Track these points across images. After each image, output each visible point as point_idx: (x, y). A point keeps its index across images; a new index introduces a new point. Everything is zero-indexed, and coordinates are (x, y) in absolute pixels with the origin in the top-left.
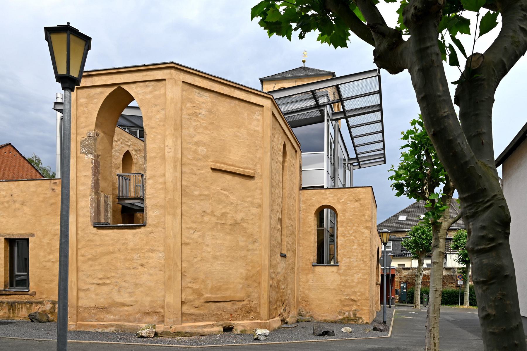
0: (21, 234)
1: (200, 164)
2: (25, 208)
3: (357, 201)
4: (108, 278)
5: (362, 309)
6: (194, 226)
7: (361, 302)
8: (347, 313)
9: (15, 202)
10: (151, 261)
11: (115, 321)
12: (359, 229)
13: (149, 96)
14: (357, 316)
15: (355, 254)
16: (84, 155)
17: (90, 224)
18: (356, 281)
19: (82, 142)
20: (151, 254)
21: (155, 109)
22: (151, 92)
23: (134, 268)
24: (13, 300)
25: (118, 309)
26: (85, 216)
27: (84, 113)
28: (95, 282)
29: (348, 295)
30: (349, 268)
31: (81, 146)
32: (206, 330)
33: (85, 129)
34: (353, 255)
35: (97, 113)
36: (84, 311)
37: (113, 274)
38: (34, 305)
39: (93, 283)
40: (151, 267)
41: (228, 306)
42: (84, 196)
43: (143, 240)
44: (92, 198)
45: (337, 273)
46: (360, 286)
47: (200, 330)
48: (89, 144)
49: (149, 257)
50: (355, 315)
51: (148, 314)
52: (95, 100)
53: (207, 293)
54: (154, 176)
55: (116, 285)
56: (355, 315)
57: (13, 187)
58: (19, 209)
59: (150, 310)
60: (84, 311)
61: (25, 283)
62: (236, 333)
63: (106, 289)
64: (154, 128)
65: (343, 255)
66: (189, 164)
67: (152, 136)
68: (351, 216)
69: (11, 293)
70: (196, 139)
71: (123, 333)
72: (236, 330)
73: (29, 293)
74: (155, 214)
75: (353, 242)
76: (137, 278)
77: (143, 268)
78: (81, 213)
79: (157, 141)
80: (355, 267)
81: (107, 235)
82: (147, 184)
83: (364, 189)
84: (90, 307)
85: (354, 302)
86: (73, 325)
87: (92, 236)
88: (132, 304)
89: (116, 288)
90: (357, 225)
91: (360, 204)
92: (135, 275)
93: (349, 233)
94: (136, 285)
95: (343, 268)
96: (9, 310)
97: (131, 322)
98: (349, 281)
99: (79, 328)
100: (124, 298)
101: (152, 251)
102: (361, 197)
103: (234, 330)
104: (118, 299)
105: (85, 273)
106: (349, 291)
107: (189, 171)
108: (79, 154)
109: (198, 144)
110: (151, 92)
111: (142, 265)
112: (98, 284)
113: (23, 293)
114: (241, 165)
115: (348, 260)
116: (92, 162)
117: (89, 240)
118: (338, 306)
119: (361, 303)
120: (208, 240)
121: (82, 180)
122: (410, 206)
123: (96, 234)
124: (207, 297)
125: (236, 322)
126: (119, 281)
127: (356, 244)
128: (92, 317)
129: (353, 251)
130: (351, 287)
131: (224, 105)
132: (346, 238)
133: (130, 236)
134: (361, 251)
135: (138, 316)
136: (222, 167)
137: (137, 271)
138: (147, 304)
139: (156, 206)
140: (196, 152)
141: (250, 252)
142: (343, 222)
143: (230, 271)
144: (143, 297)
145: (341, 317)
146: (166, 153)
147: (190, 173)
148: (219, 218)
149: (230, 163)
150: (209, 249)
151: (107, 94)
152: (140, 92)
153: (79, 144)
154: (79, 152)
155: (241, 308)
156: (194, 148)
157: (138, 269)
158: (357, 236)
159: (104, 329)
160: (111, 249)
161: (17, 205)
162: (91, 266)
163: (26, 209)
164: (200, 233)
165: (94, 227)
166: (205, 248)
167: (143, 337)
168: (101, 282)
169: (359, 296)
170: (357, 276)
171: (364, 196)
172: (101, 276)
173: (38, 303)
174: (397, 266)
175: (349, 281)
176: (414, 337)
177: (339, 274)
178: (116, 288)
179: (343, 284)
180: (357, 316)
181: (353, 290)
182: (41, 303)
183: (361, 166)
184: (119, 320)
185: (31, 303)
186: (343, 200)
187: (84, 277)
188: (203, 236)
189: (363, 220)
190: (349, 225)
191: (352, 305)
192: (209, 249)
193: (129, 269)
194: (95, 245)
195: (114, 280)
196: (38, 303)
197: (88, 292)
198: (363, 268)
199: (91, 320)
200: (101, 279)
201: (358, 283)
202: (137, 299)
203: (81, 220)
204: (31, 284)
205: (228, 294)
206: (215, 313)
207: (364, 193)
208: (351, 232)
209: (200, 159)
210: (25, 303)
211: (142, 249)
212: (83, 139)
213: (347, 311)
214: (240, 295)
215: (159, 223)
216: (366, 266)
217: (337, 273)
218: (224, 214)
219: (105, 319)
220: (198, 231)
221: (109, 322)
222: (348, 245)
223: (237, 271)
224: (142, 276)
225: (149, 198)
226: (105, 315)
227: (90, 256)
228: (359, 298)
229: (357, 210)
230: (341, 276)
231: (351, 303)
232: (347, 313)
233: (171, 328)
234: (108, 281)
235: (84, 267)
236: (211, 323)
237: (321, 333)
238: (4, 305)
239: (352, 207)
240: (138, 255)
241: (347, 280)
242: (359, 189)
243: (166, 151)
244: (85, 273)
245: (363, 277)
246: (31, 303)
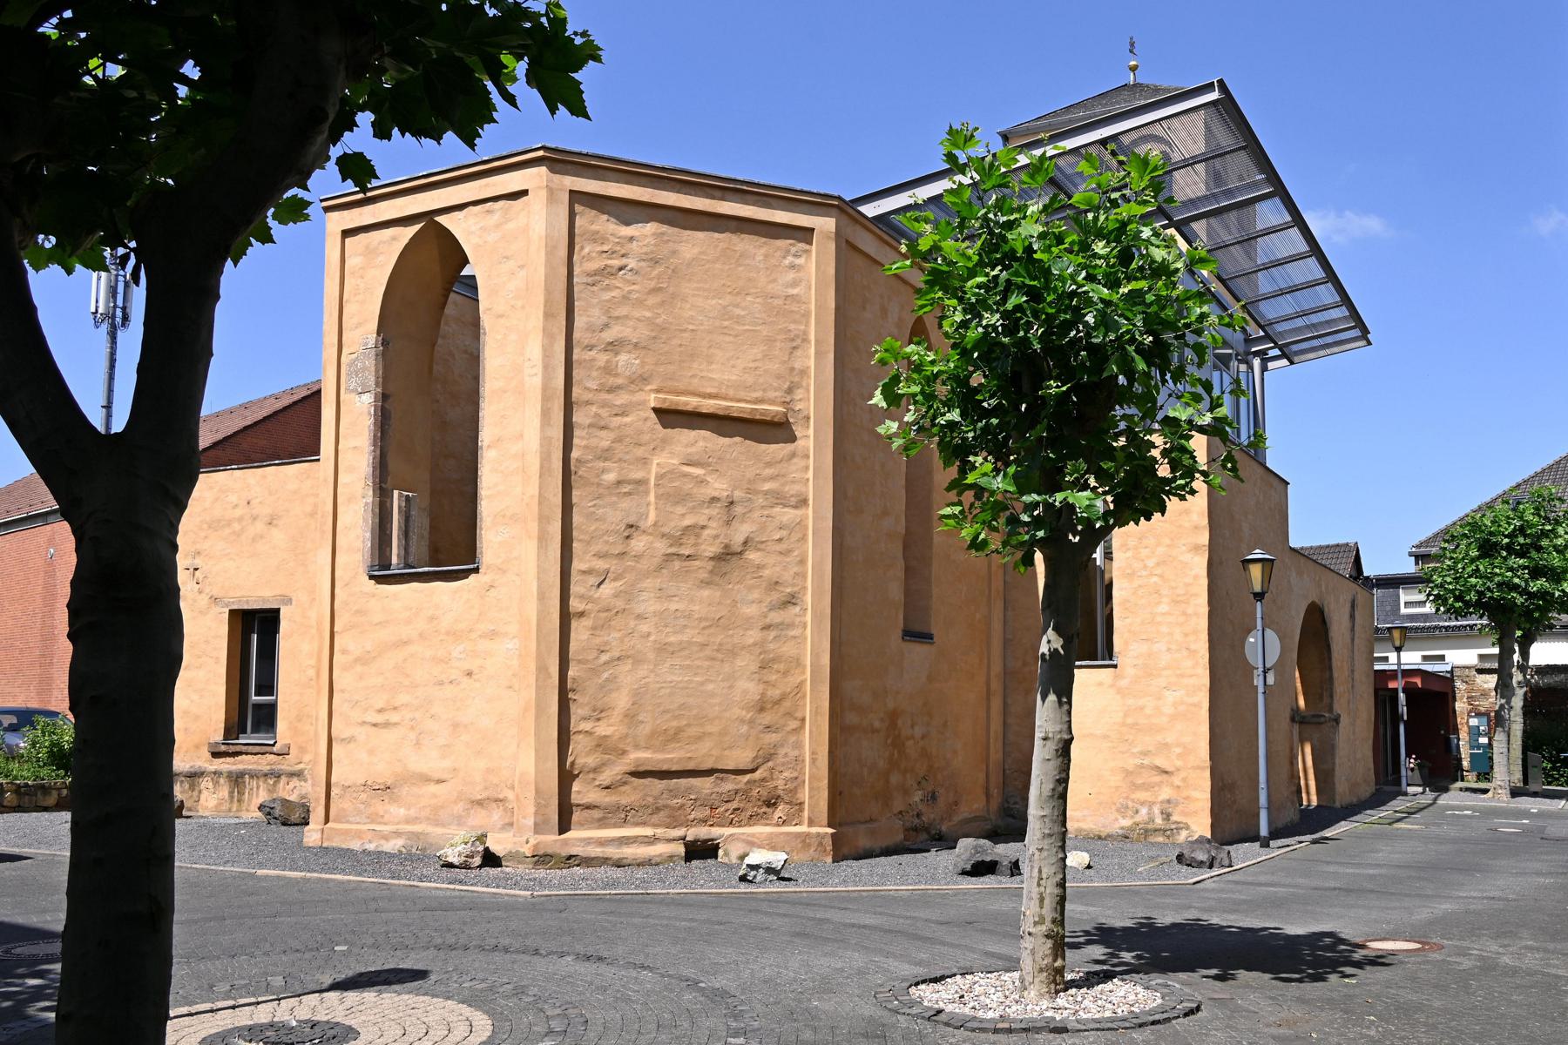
0: (264, 600)
1: (621, 399)
2: (275, 532)
6: (601, 565)
7: (1183, 774)
8: (1144, 811)
9: (255, 518)
11: (408, 822)
13: (492, 237)
14: (1174, 818)
18: (1168, 710)
19: (351, 364)
22: (498, 226)
24: (241, 767)
29: (1145, 754)
32: (630, 852)
38: (284, 779)
41: (705, 785)
45: (1112, 686)
47: (613, 852)
50: (1167, 816)
51: (480, 803)
52: (381, 258)
53: (637, 747)
55: (412, 728)
56: (1167, 816)
57: (252, 481)
58: (262, 537)
59: (484, 795)
61: (266, 718)
62: (726, 860)
63: (390, 736)
64: (501, 316)
66: (588, 403)
69: (238, 748)
70: (609, 336)
72: (726, 854)
73: (275, 749)
85: (1165, 776)
88: (443, 777)
89: (412, 736)
90: (1168, 541)
93: (1145, 567)
94: (455, 726)
96: (231, 793)
97: (443, 825)
98: (1148, 711)
101: (493, 635)
103: (721, 852)
107: (588, 421)
109: (614, 346)
111: (470, 674)
113: (264, 750)
114: (742, 394)
117: (358, 612)
118: (1117, 788)
119: (1184, 780)
120: (648, 604)
122: (1551, 467)
124: (637, 759)
126: (418, 715)
127: (1165, 600)
128: (360, 812)
129: (1159, 619)
131: (694, 244)
132: (1137, 583)
134: (1182, 619)
135: (459, 808)
136: (687, 404)
140: (608, 370)
141: (773, 634)
143: (710, 687)
145: (1127, 823)
147: (590, 426)
148: (677, 541)
149: (709, 390)
150: (644, 628)
151: (406, 241)
155: (746, 792)
156: (603, 358)
161: (260, 526)
163: (278, 536)
164: (618, 584)
165: (371, 577)
166: (632, 623)
168: (379, 719)
170: (1170, 697)
172: (380, 705)
173: (292, 775)
174: (1419, 660)
176: (1260, 885)
177: (1119, 691)
179: (1129, 721)
181: (1159, 738)
182: (298, 774)
183: (1296, 359)
184: (415, 820)
185: (278, 776)
188: (628, 594)
189: (1187, 524)
191: (1160, 784)
192: (644, 628)
193: (441, 683)
196: (292, 775)
197: (352, 745)
200: (380, 711)
204: (281, 725)
205: (703, 754)
206: (661, 803)
208: (1151, 563)
209: (619, 387)
210: (266, 775)
213: (1142, 804)
214: (741, 757)
217: (1112, 686)
220: (615, 580)
223: (731, 687)
228: (1179, 763)
231: (1157, 779)
232: (1144, 811)
234: (394, 717)
236: (649, 831)
237: (968, 867)
238: (222, 781)
240: (461, 648)
241: (1142, 708)
246: (278, 776)
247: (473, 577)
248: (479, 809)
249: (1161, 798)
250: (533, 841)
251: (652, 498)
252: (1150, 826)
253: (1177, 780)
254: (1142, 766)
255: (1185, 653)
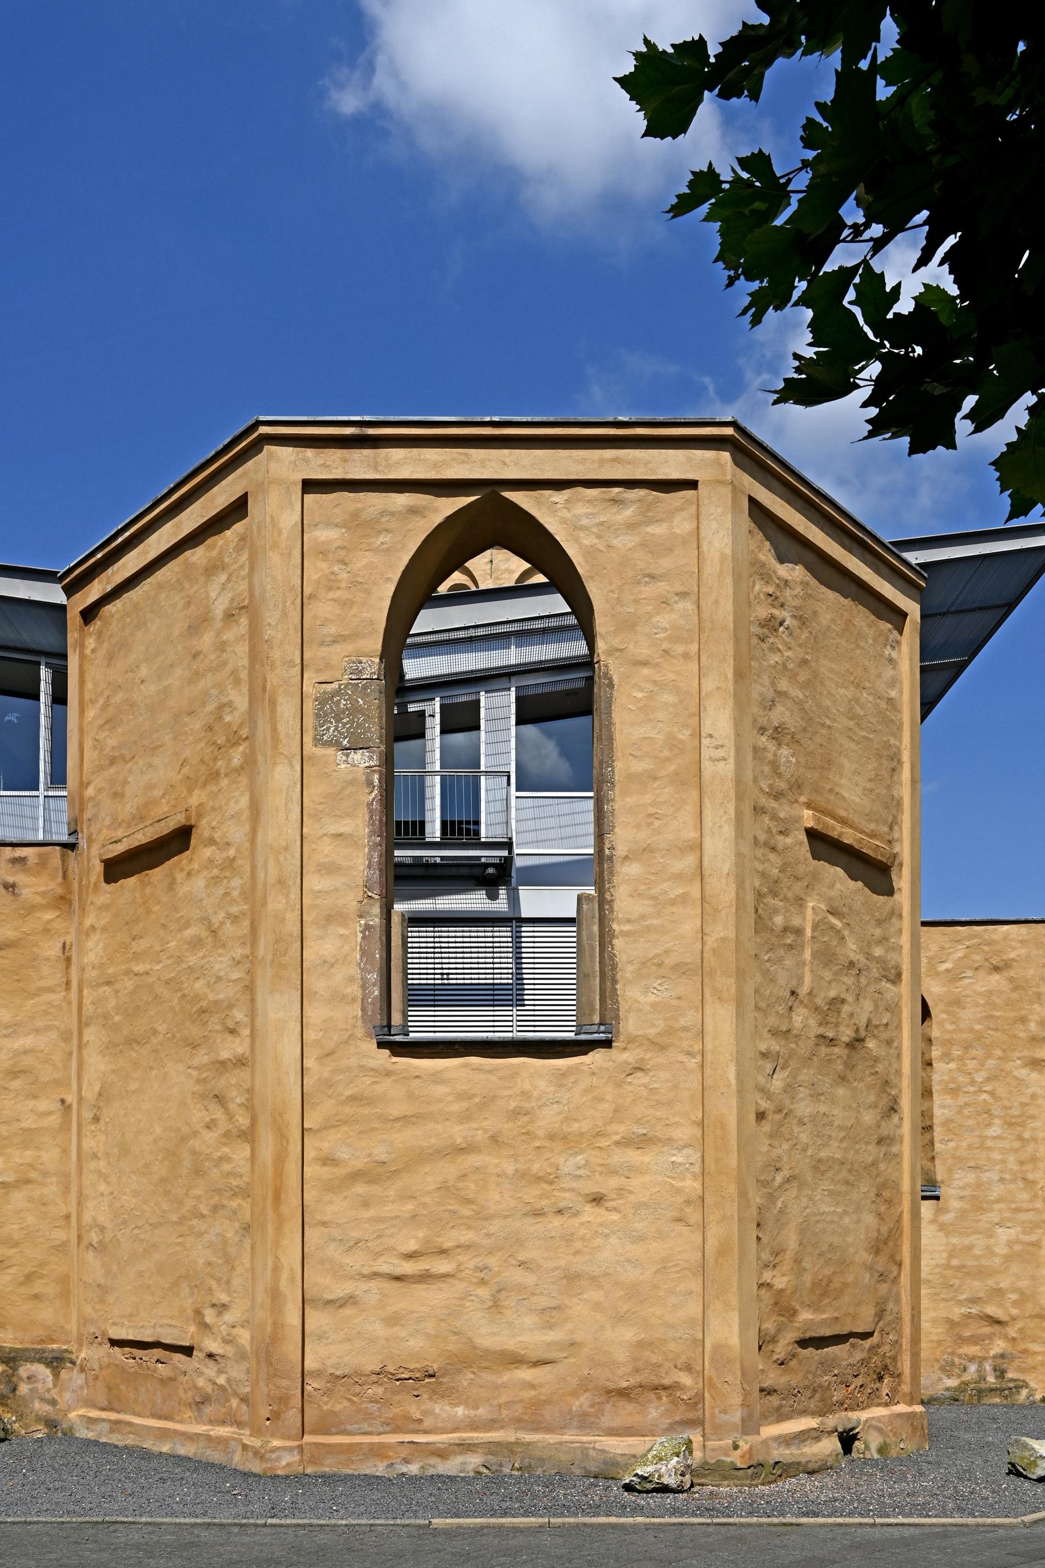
3: (996, 969)
4: (443, 1252)
5: (1025, 1351)
7: (1019, 1325)
8: (973, 1368)
10: (636, 1182)
12: (1008, 1066)
13: (624, 542)
14: (1010, 1375)
15: (996, 1156)
16: (331, 751)
17: (360, 1032)
18: (1001, 1250)
19: (323, 700)
20: (634, 1156)
21: (649, 590)
22: (631, 526)
23: (560, 1212)
25: (487, 1377)
26: (337, 998)
27: (331, 583)
28: (385, 1269)
29: (974, 1301)
30: (977, 1204)
31: (321, 717)
33: (337, 648)
34: (989, 1159)
35: (391, 588)
36: (328, 1393)
37: (466, 1236)
39: (376, 1275)
40: (639, 1206)
42: (334, 917)
43: (601, 1100)
44: (367, 927)
46: (1014, 1268)
48: (354, 710)
49: (631, 1170)
50: (1000, 1373)
51: (624, 1394)
54: (648, 850)
55: (483, 1282)
59: (633, 1381)
60: (328, 1393)
63: (434, 1296)
64: (645, 663)
65: (954, 1157)
67: (640, 695)
68: (979, 1021)
71: (512, 1480)
74: (652, 998)
75: (988, 1112)
76: (577, 1253)
77: (601, 1211)
78: (316, 983)
79: (661, 715)
80: (998, 1201)
81: (436, 1078)
82: (616, 880)
83: (1023, 929)
84: (358, 1373)
85: (997, 1328)
86: (290, 1449)
87: (368, 1081)
90: (999, 1053)
91: (1011, 980)
92: (568, 1239)
93: (973, 1082)
94: (571, 1278)
95: (955, 1204)
97: (549, 1430)
98: (977, 1252)
99: (313, 1462)
100: (524, 1333)
101: (642, 1142)
102: (1012, 955)
104: (490, 1336)
105: (335, 1233)
106: (978, 1286)
108: (309, 748)
110: (631, 526)
111: (597, 1199)
112: (398, 1278)
115: (971, 1177)
116: (370, 783)
117: (353, 1099)
118: (939, 1342)
119: (1021, 1331)
121: (324, 850)
123: (388, 1074)
125: (864, 1415)
126: (493, 1261)
127: (997, 1121)
128: (368, 1416)
129: (989, 1143)
130: (981, 1273)
132: (962, 1100)
133: (542, 1084)
134: (1016, 1144)
137: (576, 1222)
138: (621, 1355)
139: (660, 965)
142: (951, 1042)
144: (602, 1328)
145: (952, 1383)
146: (706, 764)
151: (438, 519)
152: (585, 522)
153: (309, 707)
154: (308, 739)
157: (577, 1214)
158: (1001, 1091)
159: (433, 1460)
160: (459, 1133)
162: (366, 1204)
165: (381, 1045)
167: (664, 1489)
168: (409, 1268)
169: (1015, 1303)
170: (1004, 1235)
171: (1023, 951)
172: (412, 1246)
175: (977, 1252)
178: (483, 1292)
179: (955, 1262)
180: (1010, 1375)
181: (991, 1282)
184: (492, 1424)
186: (948, 965)
187: (333, 1251)
189: (1022, 1035)
190: (973, 1052)
191: (991, 1337)
193: (539, 1213)
194: (383, 1118)
195: (468, 1261)
197: (347, 1311)
198: (1025, 1206)
199: (365, 1426)
200: (410, 1256)
201: (1008, 1259)
202: (578, 1337)
203: (315, 1014)
207: (1021, 942)
208: (979, 1078)
211: (599, 1134)
212: (329, 688)
215: (670, 1031)
216: (1035, 1197)
218: (837, 1002)
219: (428, 1423)
221: (451, 1434)
222: (970, 1122)
224: (599, 1241)
225: (626, 934)
226: (428, 1405)
227: (359, 1164)
228: (1015, 1312)
229: (999, 1001)
230: (947, 1235)
231: (987, 1330)
232: (973, 1368)
233: (736, 1447)
234: (443, 1266)
235: (334, 1208)
239: (980, 988)
241: (970, 1248)
242: (1006, 927)
243: (706, 753)
244: (335, 1233)
245: (1027, 1238)
247: (596, 1057)
248: (622, 1403)
249: (992, 1353)
250: (744, 1446)
251: (807, 954)
252: (983, 1386)
253: (1012, 1332)
254: (969, 1316)
255: (1021, 1184)
